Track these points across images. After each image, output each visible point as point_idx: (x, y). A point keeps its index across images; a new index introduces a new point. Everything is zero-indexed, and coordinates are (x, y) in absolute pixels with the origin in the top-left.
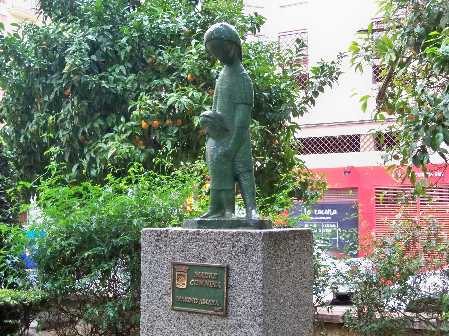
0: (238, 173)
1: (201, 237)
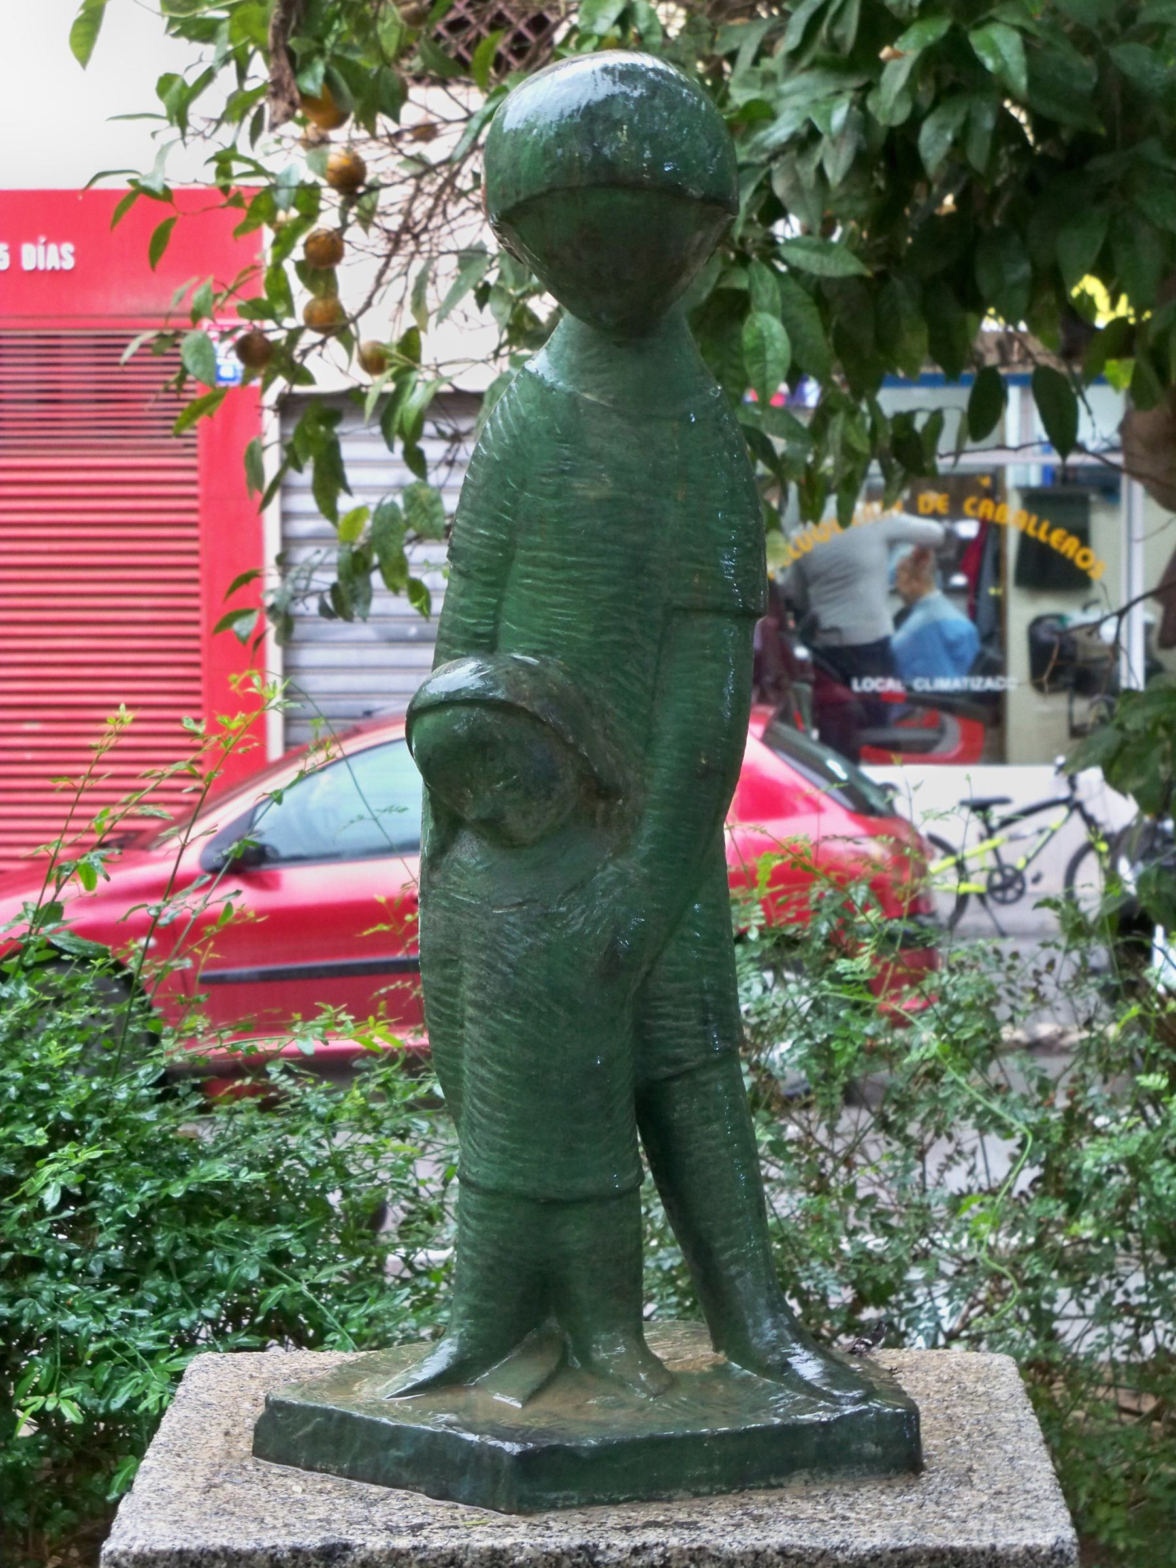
0: (666, 1071)
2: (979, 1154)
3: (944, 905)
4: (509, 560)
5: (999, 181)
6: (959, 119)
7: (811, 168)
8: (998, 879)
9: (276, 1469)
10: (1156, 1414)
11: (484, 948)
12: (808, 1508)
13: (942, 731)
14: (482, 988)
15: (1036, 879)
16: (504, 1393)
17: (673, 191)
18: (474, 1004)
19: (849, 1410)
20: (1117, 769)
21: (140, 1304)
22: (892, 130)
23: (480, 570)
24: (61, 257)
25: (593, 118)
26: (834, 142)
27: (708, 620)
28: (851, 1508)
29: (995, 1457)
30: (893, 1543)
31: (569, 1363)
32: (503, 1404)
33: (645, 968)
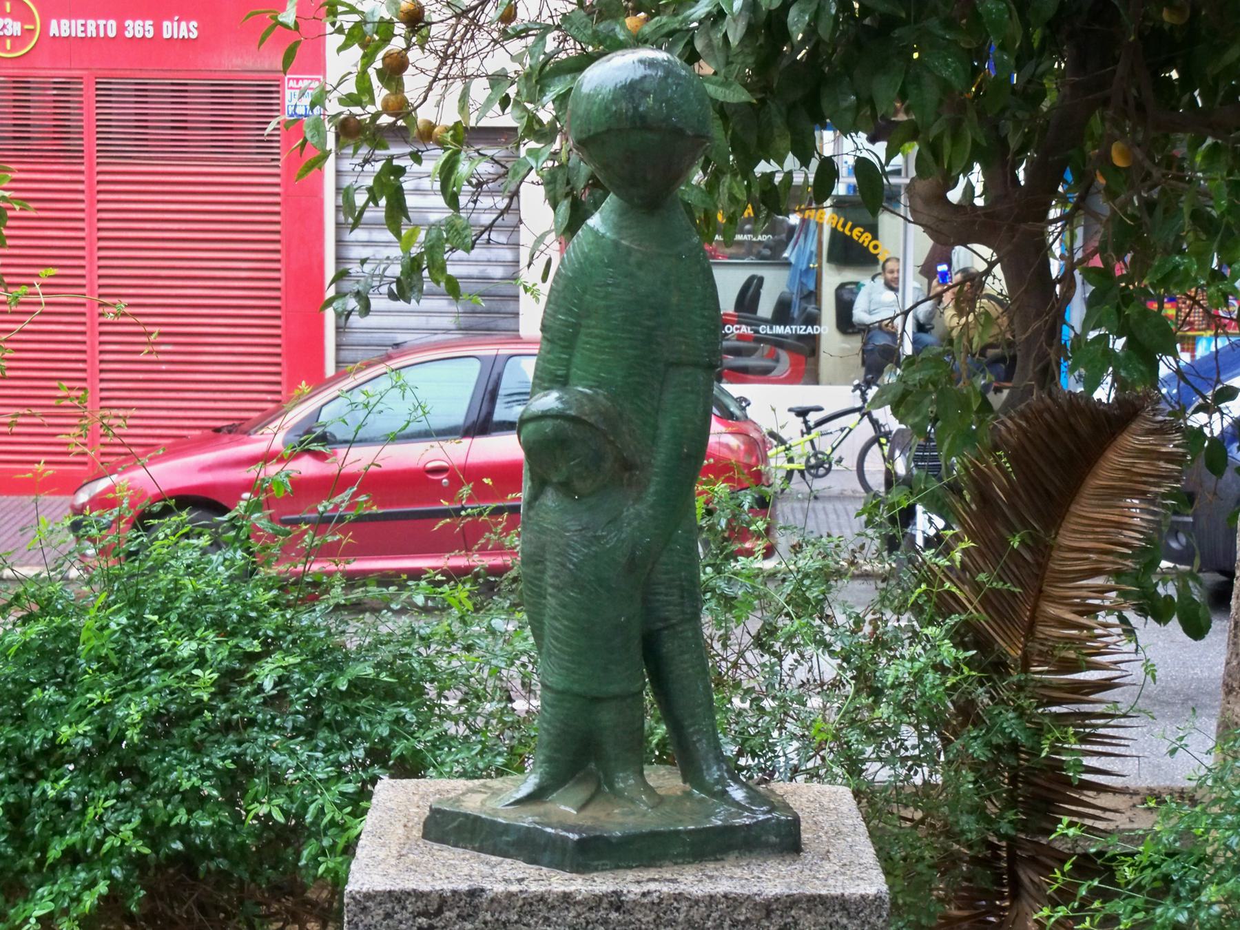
0: (661, 625)
1: (628, 918)
2: (814, 659)
3: (777, 480)
4: (575, 335)
5: (833, 11)
6: (814, 7)
7: (720, 35)
8: (813, 461)
9: (436, 846)
10: (922, 821)
11: (558, 554)
12: (738, 872)
13: (777, 360)
14: (557, 577)
15: (840, 461)
16: (566, 805)
17: (678, 132)
18: (552, 585)
19: (761, 817)
20: (902, 410)
21: (315, 748)
22: (770, 12)
23: (560, 339)
24: (189, 31)
25: (631, 90)
26: (734, 20)
27: (689, 370)
28: (763, 872)
29: (841, 844)
30: (787, 892)
31: (601, 788)
32: (566, 812)
33: (649, 567)
